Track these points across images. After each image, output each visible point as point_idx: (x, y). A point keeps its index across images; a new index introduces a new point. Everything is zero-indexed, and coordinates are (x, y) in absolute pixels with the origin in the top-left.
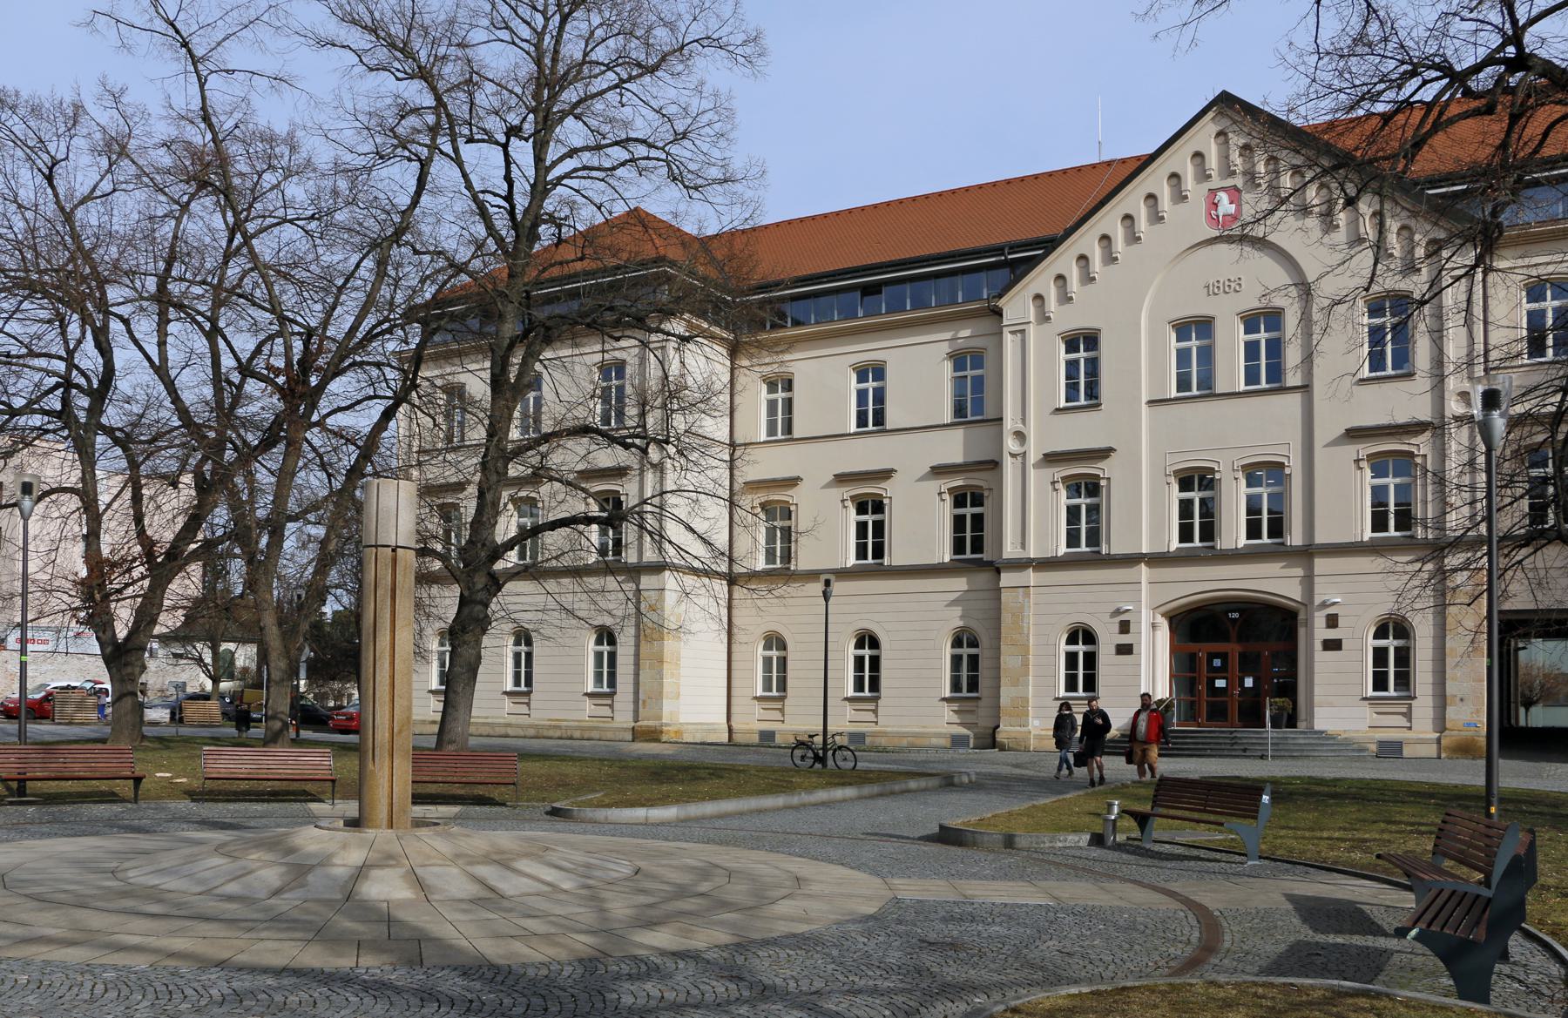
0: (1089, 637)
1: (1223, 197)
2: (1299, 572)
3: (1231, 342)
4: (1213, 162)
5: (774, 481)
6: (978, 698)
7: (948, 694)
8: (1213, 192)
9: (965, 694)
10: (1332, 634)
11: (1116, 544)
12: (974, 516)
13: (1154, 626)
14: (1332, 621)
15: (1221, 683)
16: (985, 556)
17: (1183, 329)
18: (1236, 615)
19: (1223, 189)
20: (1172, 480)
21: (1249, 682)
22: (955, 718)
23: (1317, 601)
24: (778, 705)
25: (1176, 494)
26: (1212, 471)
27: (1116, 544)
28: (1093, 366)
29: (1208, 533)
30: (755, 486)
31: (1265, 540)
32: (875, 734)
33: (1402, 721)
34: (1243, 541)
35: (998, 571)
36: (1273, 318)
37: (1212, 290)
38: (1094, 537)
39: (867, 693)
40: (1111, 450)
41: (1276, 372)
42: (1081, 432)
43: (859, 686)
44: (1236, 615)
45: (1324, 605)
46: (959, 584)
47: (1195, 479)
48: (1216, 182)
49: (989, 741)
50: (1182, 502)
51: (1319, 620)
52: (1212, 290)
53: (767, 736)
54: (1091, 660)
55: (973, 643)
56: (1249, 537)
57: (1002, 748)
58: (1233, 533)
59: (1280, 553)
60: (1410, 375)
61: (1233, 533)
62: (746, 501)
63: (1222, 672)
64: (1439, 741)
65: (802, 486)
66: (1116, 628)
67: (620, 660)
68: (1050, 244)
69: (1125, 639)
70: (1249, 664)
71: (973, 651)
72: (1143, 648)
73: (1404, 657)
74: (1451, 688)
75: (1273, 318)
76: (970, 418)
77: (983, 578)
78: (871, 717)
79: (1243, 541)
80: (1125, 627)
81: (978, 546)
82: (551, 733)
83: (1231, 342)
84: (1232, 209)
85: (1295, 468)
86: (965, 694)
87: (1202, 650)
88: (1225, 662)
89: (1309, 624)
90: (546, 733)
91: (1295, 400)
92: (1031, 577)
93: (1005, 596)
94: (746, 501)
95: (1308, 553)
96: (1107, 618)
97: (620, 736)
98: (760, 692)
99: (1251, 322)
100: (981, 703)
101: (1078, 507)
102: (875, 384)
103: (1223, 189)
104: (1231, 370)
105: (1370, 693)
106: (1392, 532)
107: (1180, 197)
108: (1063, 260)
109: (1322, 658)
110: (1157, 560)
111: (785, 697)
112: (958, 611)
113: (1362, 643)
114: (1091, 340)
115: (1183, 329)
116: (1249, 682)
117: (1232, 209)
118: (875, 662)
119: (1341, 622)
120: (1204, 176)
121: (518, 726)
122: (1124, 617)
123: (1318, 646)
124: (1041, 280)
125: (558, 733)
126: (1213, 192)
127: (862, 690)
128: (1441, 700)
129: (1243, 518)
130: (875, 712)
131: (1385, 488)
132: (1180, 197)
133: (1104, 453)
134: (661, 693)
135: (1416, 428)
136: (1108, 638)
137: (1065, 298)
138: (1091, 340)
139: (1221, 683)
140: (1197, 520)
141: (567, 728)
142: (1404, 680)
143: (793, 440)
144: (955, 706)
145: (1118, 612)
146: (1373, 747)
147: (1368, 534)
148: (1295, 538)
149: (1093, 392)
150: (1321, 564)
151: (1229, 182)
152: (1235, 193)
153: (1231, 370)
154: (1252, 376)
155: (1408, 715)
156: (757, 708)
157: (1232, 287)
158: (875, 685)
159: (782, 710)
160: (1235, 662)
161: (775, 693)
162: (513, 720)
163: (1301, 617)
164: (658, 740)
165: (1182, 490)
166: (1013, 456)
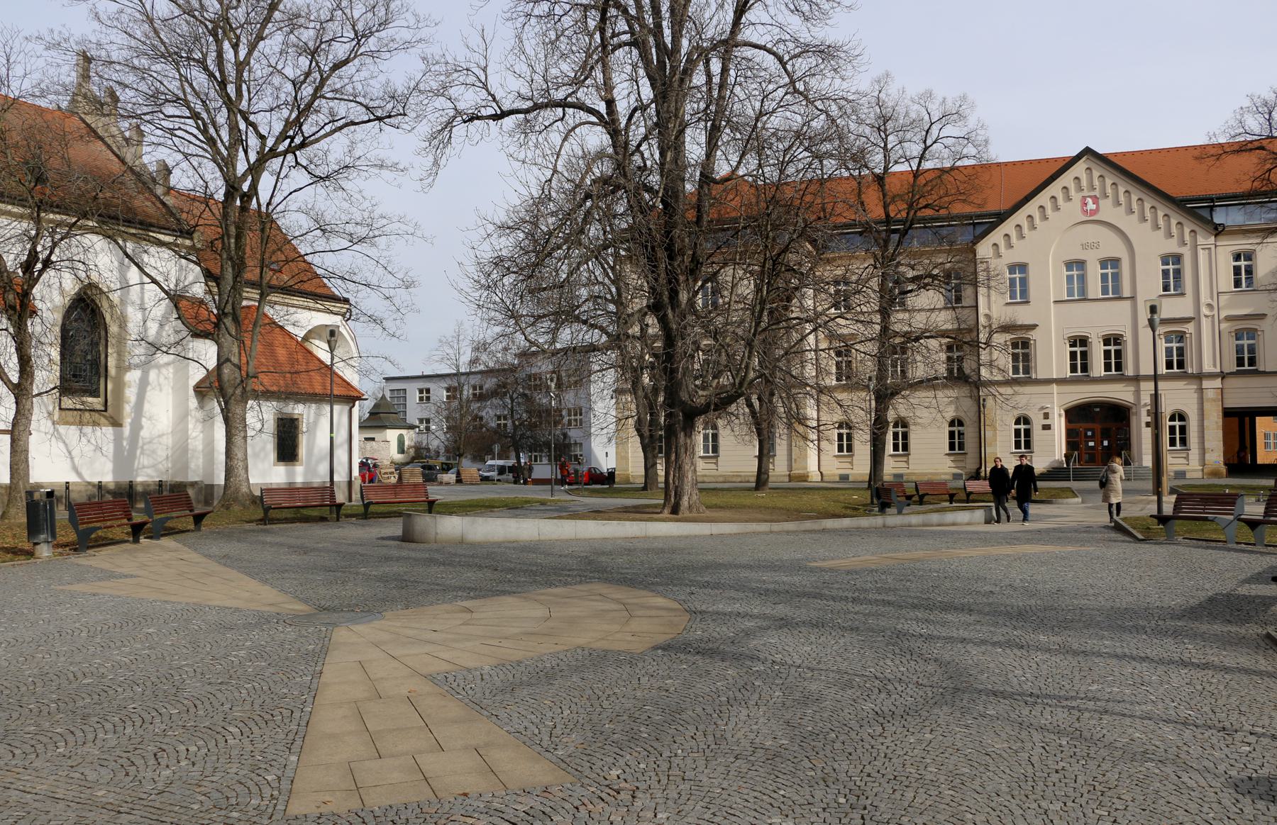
0: (1027, 421)
1: (1089, 201)
2: (1132, 389)
3: (1094, 273)
4: (1084, 183)
5: (1175, 319)
7: (948, 452)
8: (1084, 198)
9: (957, 451)
11: (1040, 372)
12: (1249, 346)
13: (1060, 415)
15: (1091, 444)
17: (1069, 265)
18: (1098, 410)
19: (1090, 197)
20: (1067, 342)
21: (1106, 443)
22: (952, 465)
26: (1122, 336)
28: (1024, 282)
29: (1085, 368)
30: (1165, 322)
31: (1079, 373)
32: (908, 474)
33: (1184, 461)
37: (1085, 247)
40: (1265, 315)
41: (1117, 289)
44: (1098, 410)
48: (1086, 193)
50: (1071, 352)
52: (1085, 247)
53: (844, 478)
54: (1028, 432)
55: (961, 424)
56: (1167, 368)
58: (1098, 368)
59: (1122, 379)
60: (1183, 294)
61: (1098, 368)
62: (1161, 330)
63: (1092, 438)
64: (1203, 470)
66: (1042, 416)
68: (1001, 217)
69: (1047, 422)
70: (1106, 434)
74: (1207, 445)
75: (1177, 259)
78: (905, 465)
79: (1103, 373)
80: (1046, 416)
82: (734, 479)
83: (1094, 273)
84: (1094, 207)
85: (1128, 338)
87: (1080, 426)
88: (1093, 433)
89: (1138, 414)
90: (730, 479)
91: (1127, 304)
94: (1161, 330)
96: (1036, 411)
97: (781, 479)
99: (1104, 263)
100: (968, 456)
103: (1090, 197)
104: (1095, 289)
105: (837, 453)
107: (1068, 199)
108: (1008, 227)
114: (1023, 267)
115: (1069, 265)
116: (1106, 443)
117: (1094, 207)
120: (1080, 189)
121: (713, 476)
122: (1046, 411)
123: (1143, 425)
124: (996, 236)
125: (739, 480)
126: (1084, 198)
128: (1203, 451)
130: (907, 462)
132: (1068, 199)
133: (1034, 327)
135: (1186, 320)
136: (1037, 422)
137: (1010, 246)
138: (1023, 267)
139: (1091, 444)
140: (1079, 362)
141: (745, 476)
142: (1184, 441)
143: (1085, 300)
144: (952, 458)
145: (1042, 408)
147: (1069, 374)
148: (1130, 371)
151: (1092, 194)
152: (1095, 200)
153: (1095, 289)
154: (1105, 291)
155: (1187, 458)
156: (836, 463)
158: (905, 447)
159: (851, 463)
160: (1098, 434)
162: (707, 473)
163: (1134, 410)
164: (806, 481)
165: (1105, 345)
166: (1206, 316)
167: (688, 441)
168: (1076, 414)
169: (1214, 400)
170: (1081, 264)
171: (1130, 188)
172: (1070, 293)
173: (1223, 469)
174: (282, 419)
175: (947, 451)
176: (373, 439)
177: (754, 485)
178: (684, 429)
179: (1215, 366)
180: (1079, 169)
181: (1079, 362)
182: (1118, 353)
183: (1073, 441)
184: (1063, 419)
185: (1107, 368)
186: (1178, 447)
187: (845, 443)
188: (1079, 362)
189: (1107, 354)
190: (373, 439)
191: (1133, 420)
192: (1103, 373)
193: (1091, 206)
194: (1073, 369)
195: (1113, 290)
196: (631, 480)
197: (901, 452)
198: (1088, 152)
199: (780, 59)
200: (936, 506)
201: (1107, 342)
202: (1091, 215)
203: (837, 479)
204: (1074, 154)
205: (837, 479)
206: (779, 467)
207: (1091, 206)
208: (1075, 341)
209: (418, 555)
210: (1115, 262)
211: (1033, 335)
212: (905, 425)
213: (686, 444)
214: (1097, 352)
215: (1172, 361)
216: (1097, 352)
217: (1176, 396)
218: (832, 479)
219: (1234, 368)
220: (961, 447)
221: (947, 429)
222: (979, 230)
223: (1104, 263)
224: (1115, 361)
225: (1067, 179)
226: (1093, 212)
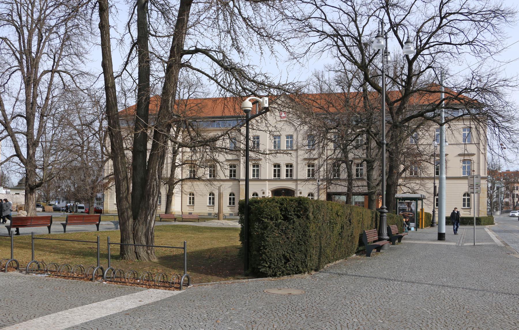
2: (295, 184)
9: (466, 207)
11: (262, 177)
13: (269, 193)
16: (236, 178)
22: (230, 210)
23: (298, 189)
24: (192, 207)
25: (273, 168)
27: (262, 177)
29: (279, 176)
34: (285, 178)
35: (239, 181)
36: (291, 136)
38: (258, 175)
39: (191, 205)
43: (190, 203)
45: (299, 190)
46: (231, 183)
51: (298, 192)
55: (234, 195)
58: (283, 176)
59: (292, 180)
61: (283, 176)
67: (215, 199)
71: (234, 197)
73: (213, 199)
77: (236, 183)
78: (213, 210)
79: (285, 178)
81: (235, 176)
85: (294, 165)
86: (232, 205)
89: (296, 193)
93: (241, 186)
95: (296, 180)
96: (260, 191)
98: (188, 204)
99: (288, 137)
101: (255, 170)
102: (361, 138)
106: (289, 178)
110: (269, 180)
112: (230, 189)
118: (193, 198)
127: (190, 204)
129: (285, 173)
130: (213, 209)
131: (288, 169)
144: (230, 208)
145: (262, 190)
147: (273, 178)
148: (294, 177)
150: (299, 182)
155: (470, 212)
156: (188, 208)
158: (193, 203)
159: (193, 208)
161: (212, 205)
163: (295, 192)
167: (31, 196)
173: (53, 210)
175: (228, 205)
176: (18, 194)
178: (30, 193)
179: (485, 174)
181: (277, 173)
182: (291, 170)
185: (287, 176)
186: (191, 205)
187: (232, 201)
188: (277, 173)
189: (287, 171)
190: (18, 194)
194: (275, 176)
196: (109, 212)
197: (466, 207)
199: (71, 76)
201: (287, 166)
203: (207, 215)
205: (207, 215)
208: (288, 165)
211: (260, 162)
212: (193, 195)
213: (30, 197)
215: (310, 174)
219: (306, 177)
220: (234, 203)
221: (208, 196)
223: (288, 137)
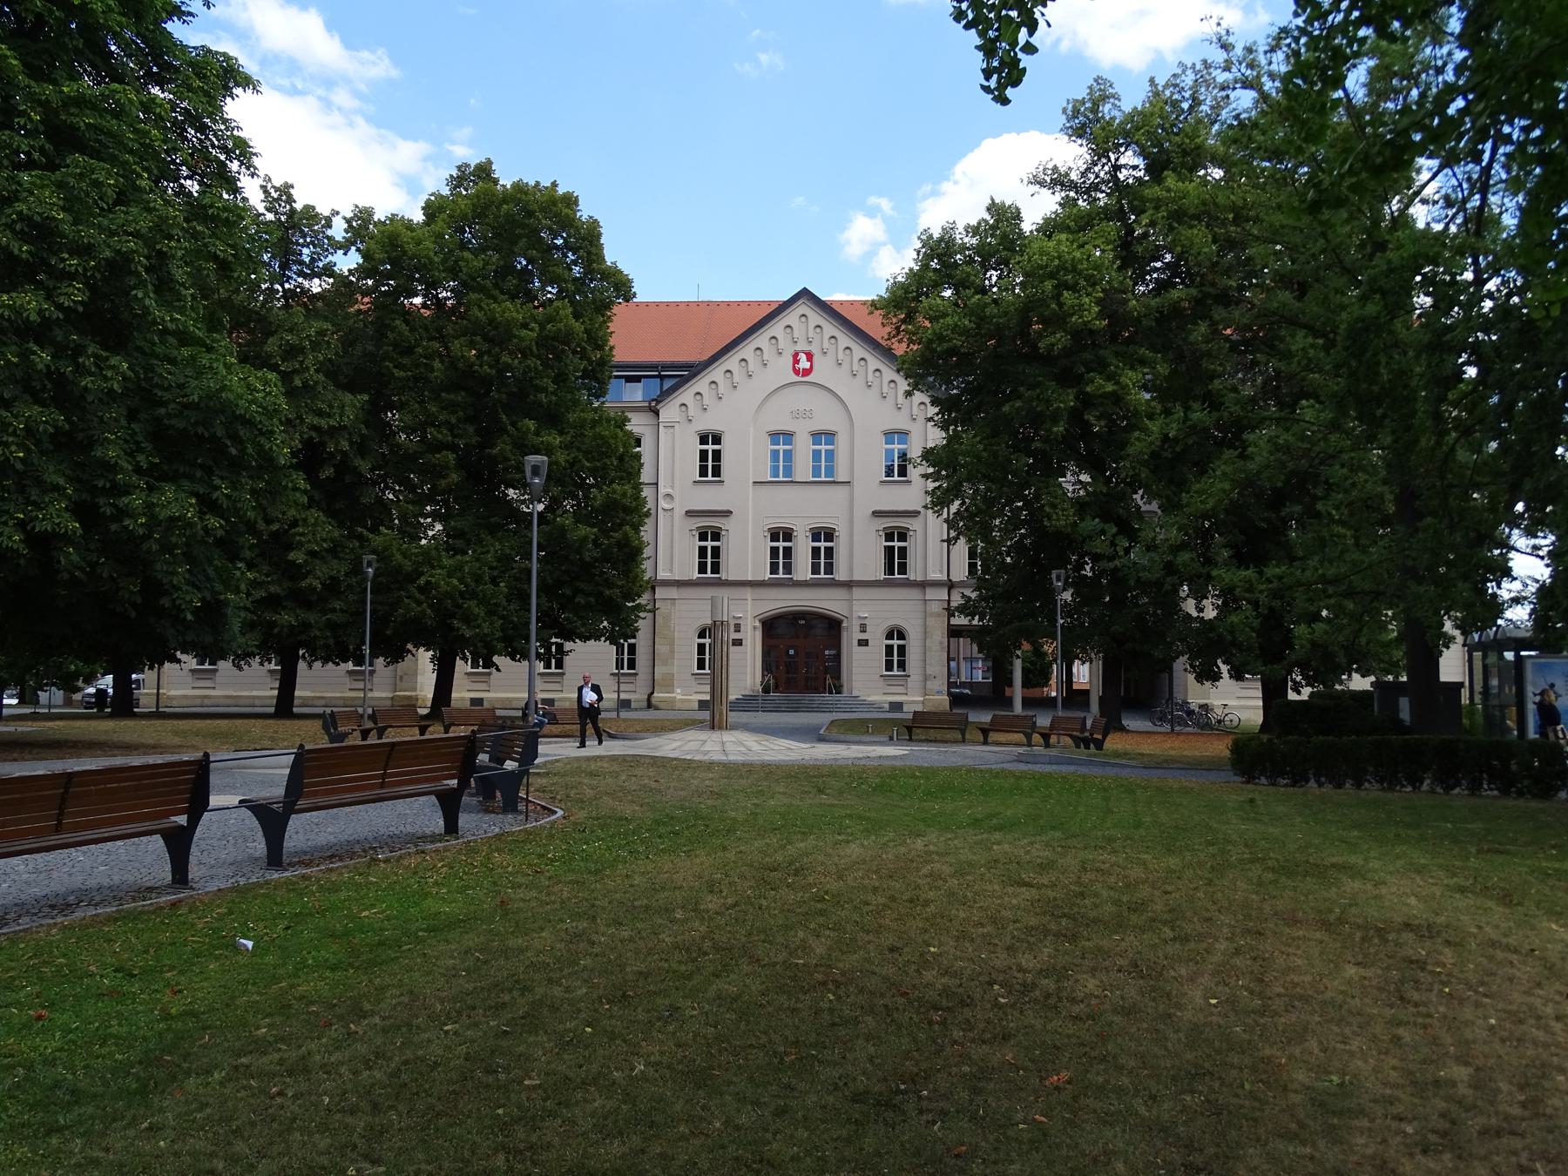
1: (803, 357)
3: (803, 449)
5: (897, 512)
6: (636, 674)
10: (863, 636)
11: (730, 571)
13: (755, 628)
14: (863, 629)
37: (797, 415)
42: (709, 497)
47: (781, 534)
49: (645, 703)
55: (901, 636)
57: (657, 709)
58: (803, 569)
65: (732, 517)
72: (748, 642)
76: (823, 479)
79: (810, 576)
83: (803, 449)
84: (808, 365)
90: (310, 703)
92: (673, 593)
99: (817, 436)
104: (803, 470)
108: (701, 384)
109: (857, 650)
111: (563, 674)
113: (879, 643)
115: (775, 436)
117: (808, 365)
119: (868, 629)
123: (855, 643)
124: (686, 395)
134: (416, 670)
146: (887, 706)
149: (717, 471)
153: (803, 470)
157: (807, 415)
163: (844, 625)
168: (771, 626)
169: (939, 615)
170: (788, 436)
171: (836, 333)
172: (775, 472)
174: (819, 688)
177: (272, 710)
180: (791, 317)
183: (771, 660)
184: (759, 634)
185: (816, 569)
191: (844, 635)
192: (810, 576)
193: (804, 364)
195: (826, 475)
198: (805, 294)
200: (118, 761)
201: (816, 536)
202: (804, 375)
204: (786, 298)
206: (461, 693)
207: (804, 364)
209: (776, 748)
210: (830, 436)
214: (803, 548)
216: (803, 548)
217: (899, 609)
218: (686, 706)
222: (668, 384)
224: (824, 558)
225: (777, 328)
226: (807, 372)
